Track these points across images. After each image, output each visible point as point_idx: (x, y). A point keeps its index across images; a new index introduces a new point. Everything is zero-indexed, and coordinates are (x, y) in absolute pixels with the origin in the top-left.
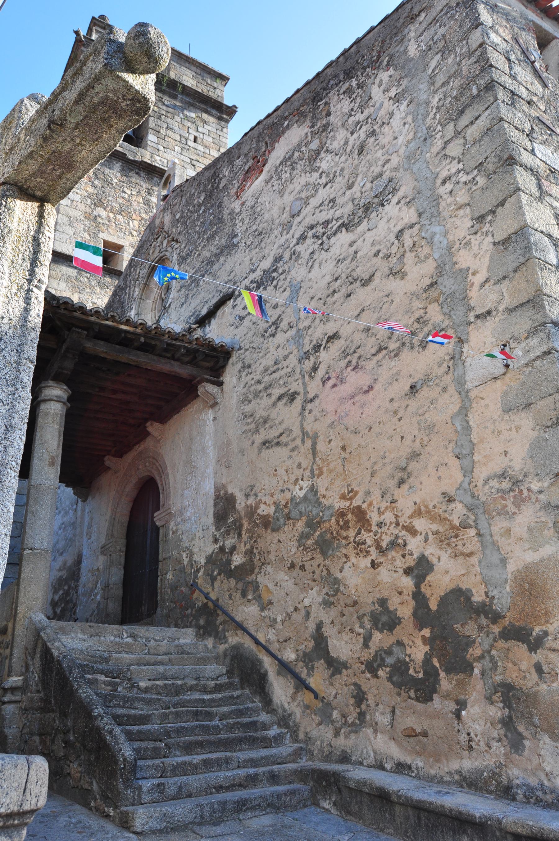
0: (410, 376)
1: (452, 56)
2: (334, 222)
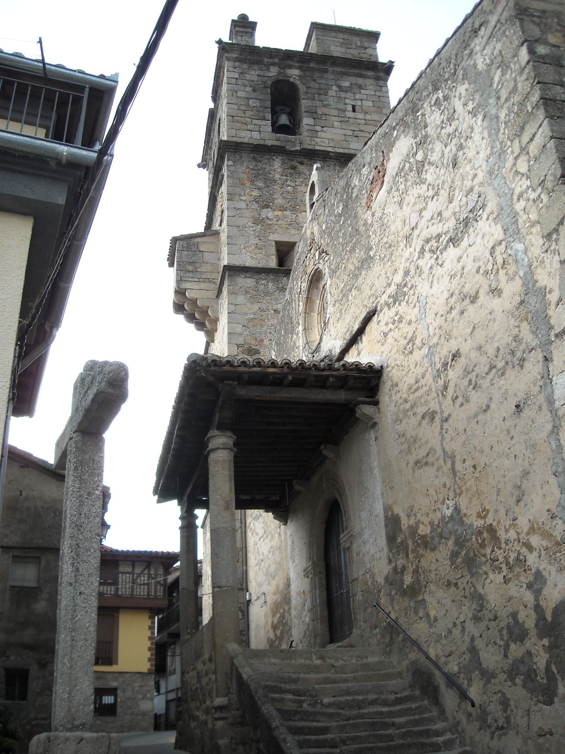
0: (515, 395)
1: (509, 72)
2: (444, 236)
